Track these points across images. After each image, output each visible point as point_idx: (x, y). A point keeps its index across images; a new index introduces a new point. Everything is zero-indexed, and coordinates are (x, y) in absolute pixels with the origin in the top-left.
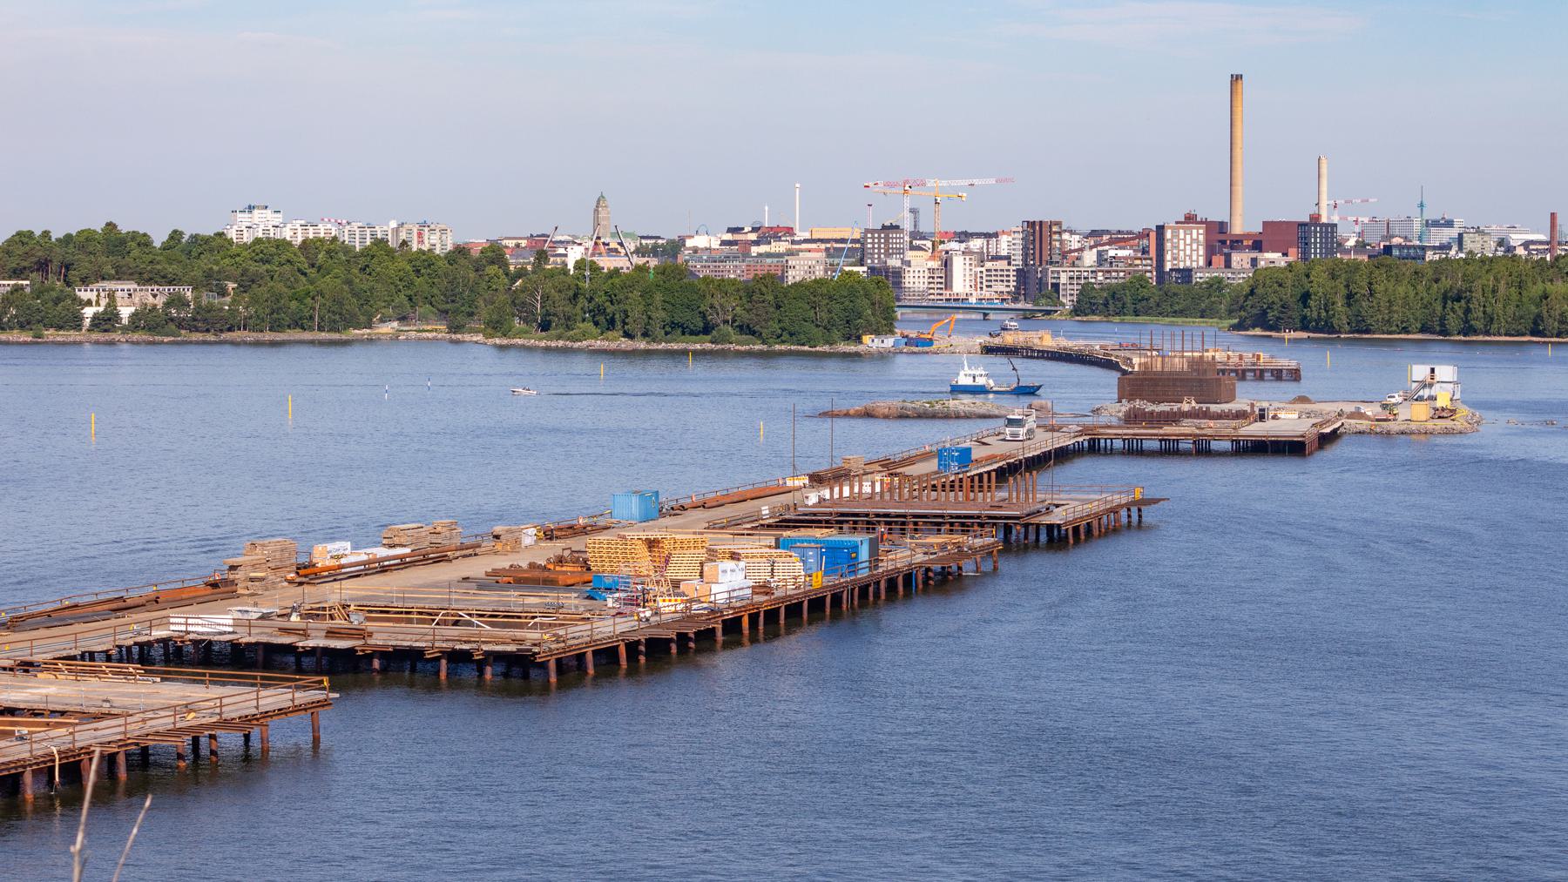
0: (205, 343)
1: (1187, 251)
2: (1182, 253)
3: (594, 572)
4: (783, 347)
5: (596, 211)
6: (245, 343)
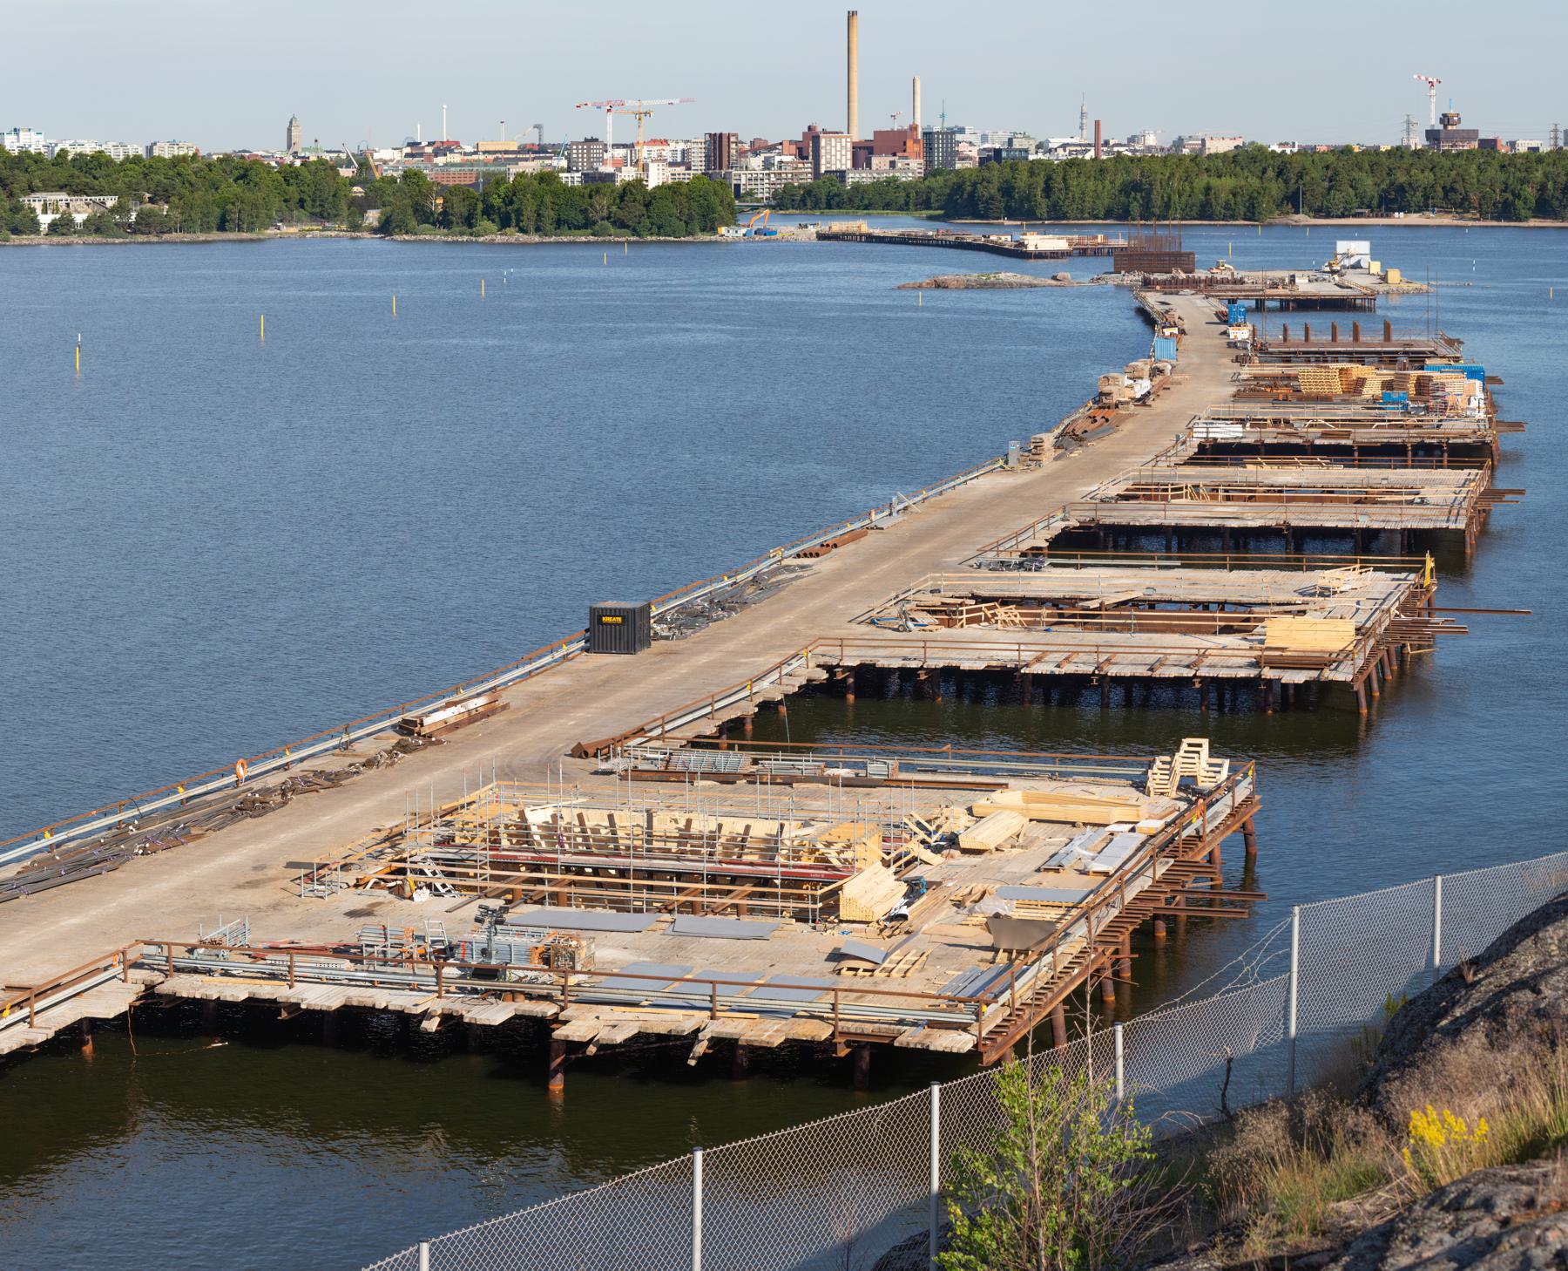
0: (149, 243)
1: (836, 156)
3: (1468, 525)
4: (654, 238)
5: (289, 130)
6: (183, 243)
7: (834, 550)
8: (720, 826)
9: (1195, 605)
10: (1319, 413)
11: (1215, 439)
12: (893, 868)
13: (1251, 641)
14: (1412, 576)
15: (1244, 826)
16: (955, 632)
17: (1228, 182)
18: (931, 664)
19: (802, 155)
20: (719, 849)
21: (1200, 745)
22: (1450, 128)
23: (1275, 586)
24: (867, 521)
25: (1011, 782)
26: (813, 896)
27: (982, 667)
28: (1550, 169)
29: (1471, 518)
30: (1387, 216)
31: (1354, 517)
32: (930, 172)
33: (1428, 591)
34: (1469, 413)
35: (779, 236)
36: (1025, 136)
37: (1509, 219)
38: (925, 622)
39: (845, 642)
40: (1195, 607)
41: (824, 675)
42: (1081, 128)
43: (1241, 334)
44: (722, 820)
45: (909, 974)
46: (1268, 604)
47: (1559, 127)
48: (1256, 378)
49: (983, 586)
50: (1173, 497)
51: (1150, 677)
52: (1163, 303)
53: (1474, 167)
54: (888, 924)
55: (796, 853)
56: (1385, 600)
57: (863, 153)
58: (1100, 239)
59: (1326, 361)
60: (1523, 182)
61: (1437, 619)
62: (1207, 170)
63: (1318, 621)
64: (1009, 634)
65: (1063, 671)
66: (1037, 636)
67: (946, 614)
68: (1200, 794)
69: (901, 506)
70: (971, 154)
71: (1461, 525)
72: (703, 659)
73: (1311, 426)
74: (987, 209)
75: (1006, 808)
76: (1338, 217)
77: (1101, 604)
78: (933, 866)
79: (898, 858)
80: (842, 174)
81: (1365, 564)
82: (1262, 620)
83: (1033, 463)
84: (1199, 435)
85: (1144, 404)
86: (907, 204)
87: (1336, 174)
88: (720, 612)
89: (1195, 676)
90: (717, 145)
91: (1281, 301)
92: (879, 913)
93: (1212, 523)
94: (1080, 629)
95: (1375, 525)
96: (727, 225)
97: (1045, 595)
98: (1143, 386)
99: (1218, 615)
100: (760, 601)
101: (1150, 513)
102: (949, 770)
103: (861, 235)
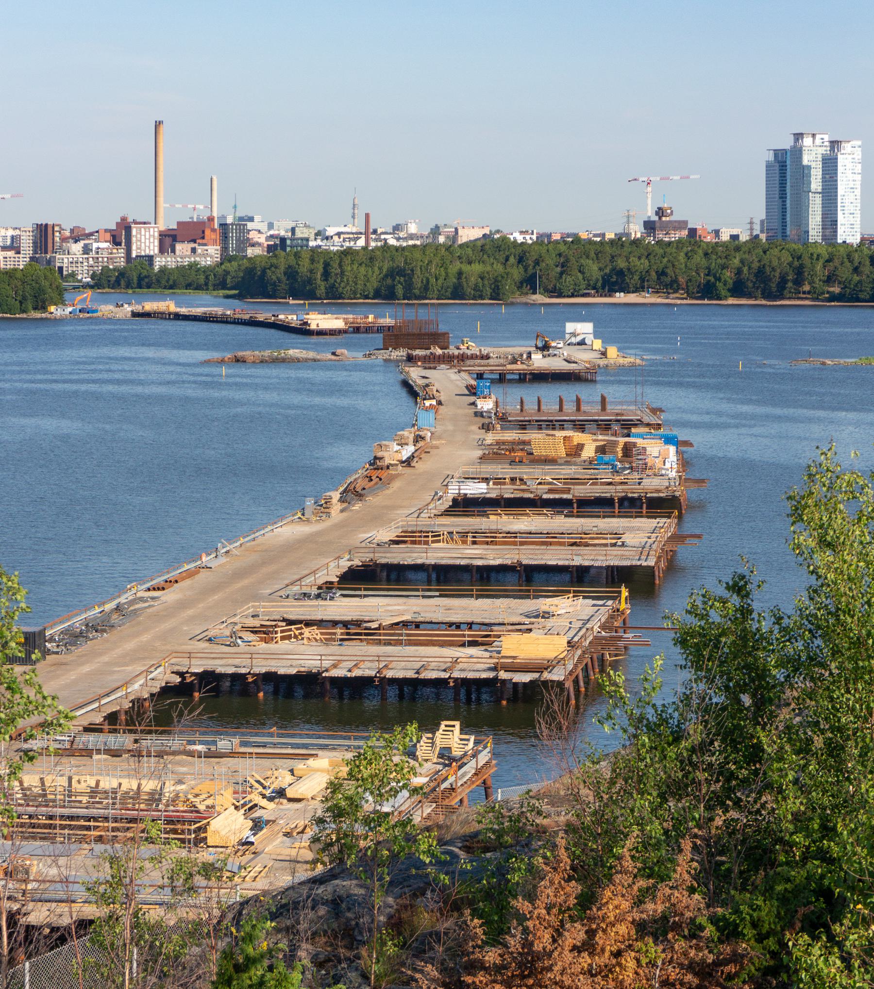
2: (143, 245)
3: (656, 563)
7: (176, 585)
8: (120, 784)
9: (450, 624)
10: (547, 474)
11: (466, 494)
12: (242, 811)
13: (491, 652)
14: (610, 603)
15: (484, 782)
16: (272, 646)
17: (477, 268)
18: (256, 670)
19: (116, 242)
20: (118, 801)
21: (454, 726)
22: (664, 219)
23: (509, 610)
24: (199, 563)
25: (320, 753)
26: (189, 830)
27: (294, 672)
28: (746, 256)
29: (659, 558)
30: (610, 296)
31: (570, 556)
32: (226, 258)
33: (623, 614)
34: (663, 472)
35: (99, 314)
36: (306, 226)
37: (710, 299)
38: (250, 639)
39: (192, 655)
40: (450, 626)
41: (178, 679)
42: (353, 217)
43: (486, 405)
44: (121, 780)
45: (257, 879)
46: (504, 624)
47: (754, 220)
48: (498, 443)
49: (291, 612)
50: (433, 542)
51: (417, 679)
52: (424, 377)
53: (682, 254)
54: (240, 847)
55: (174, 800)
56: (589, 620)
57: (168, 240)
58: (371, 318)
59: (554, 429)
60: (724, 267)
61: (629, 635)
62: (460, 258)
63: (540, 637)
64: (313, 648)
65: (354, 674)
66: (334, 649)
67: (265, 632)
68: (453, 759)
69: (225, 550)
70: (260, 241)
71: (651, 562)
72: (86, 668)
73: (540, 484)
74: (275, 291)
75: (317, 770)
76: (568, 296)
77: (380, 625)
78: (269, 809)
79: (244, 805)
80: (150, 258)
81: (576, 594)
82: (499, 636)
83: (324, 515)
84: (453, 491)
85: (409, 465)
86: (206, 284)
87: (567, 260)
88: (94, 634)
89: (450, 678)
90: (43, 233)
91: (520, 374)
92: (234, 840)
93: (463, 562)
94: (365, 643)
95: (586, 563)
96: (55, 304)
97: (337, 618)
98: (408, 451)
99: (467, 633)
100: (123, 624)
101: (416, 555)
102: (275, 745)
103: (170, 314)
